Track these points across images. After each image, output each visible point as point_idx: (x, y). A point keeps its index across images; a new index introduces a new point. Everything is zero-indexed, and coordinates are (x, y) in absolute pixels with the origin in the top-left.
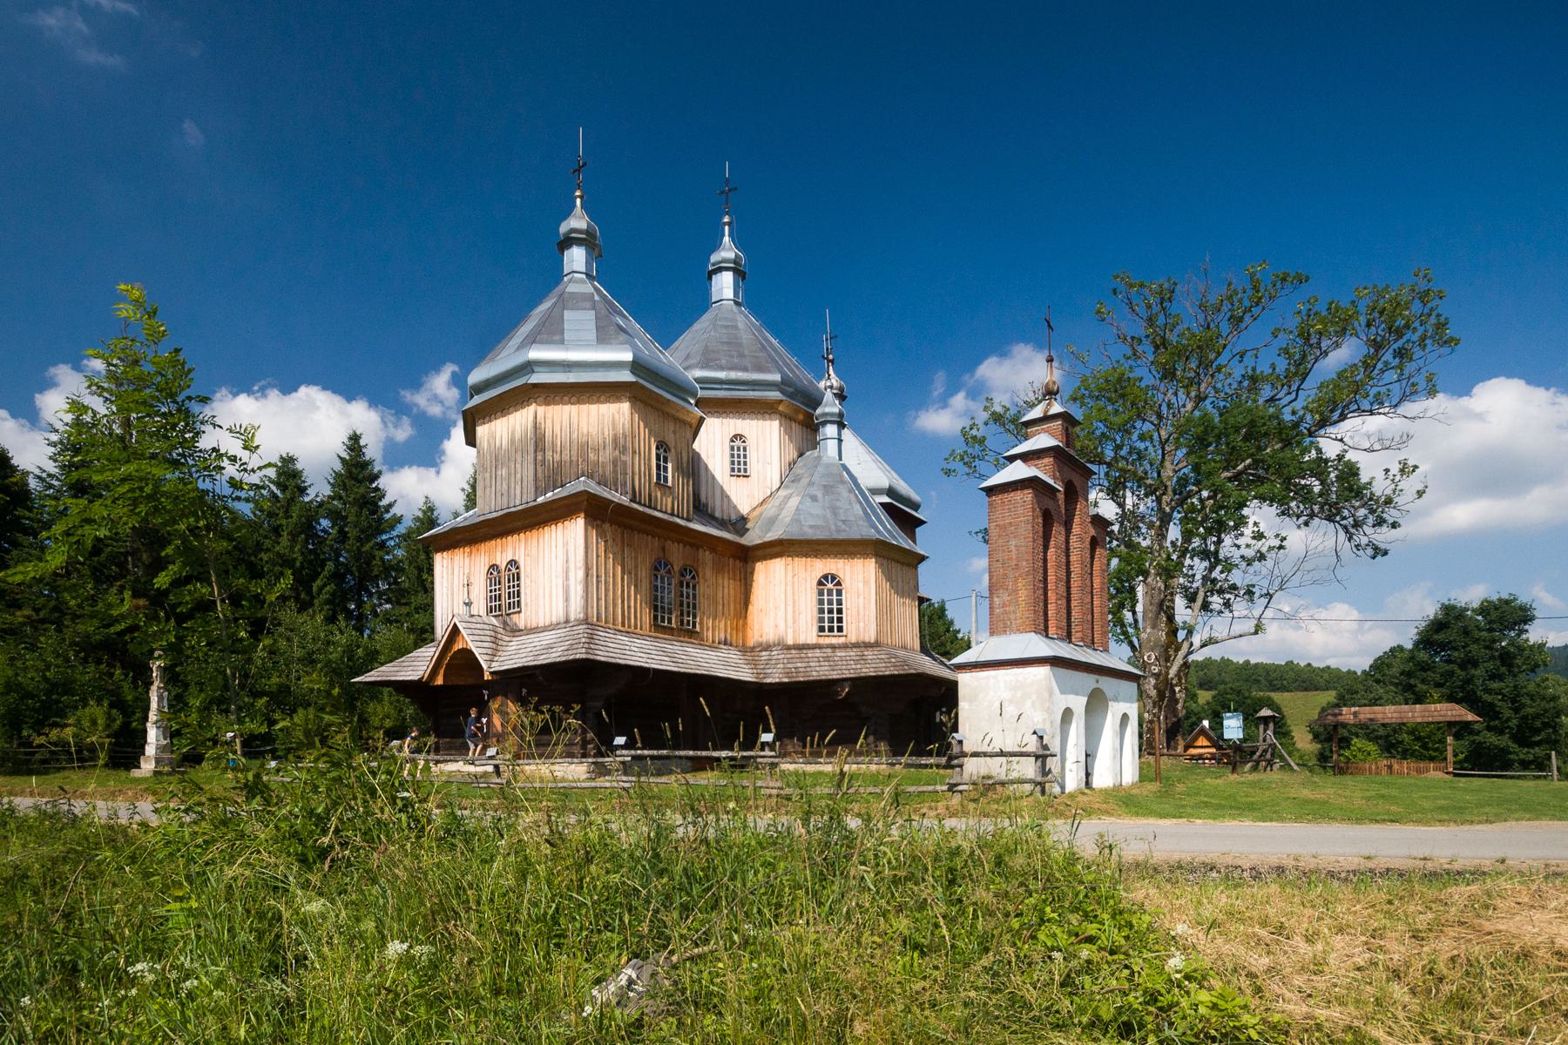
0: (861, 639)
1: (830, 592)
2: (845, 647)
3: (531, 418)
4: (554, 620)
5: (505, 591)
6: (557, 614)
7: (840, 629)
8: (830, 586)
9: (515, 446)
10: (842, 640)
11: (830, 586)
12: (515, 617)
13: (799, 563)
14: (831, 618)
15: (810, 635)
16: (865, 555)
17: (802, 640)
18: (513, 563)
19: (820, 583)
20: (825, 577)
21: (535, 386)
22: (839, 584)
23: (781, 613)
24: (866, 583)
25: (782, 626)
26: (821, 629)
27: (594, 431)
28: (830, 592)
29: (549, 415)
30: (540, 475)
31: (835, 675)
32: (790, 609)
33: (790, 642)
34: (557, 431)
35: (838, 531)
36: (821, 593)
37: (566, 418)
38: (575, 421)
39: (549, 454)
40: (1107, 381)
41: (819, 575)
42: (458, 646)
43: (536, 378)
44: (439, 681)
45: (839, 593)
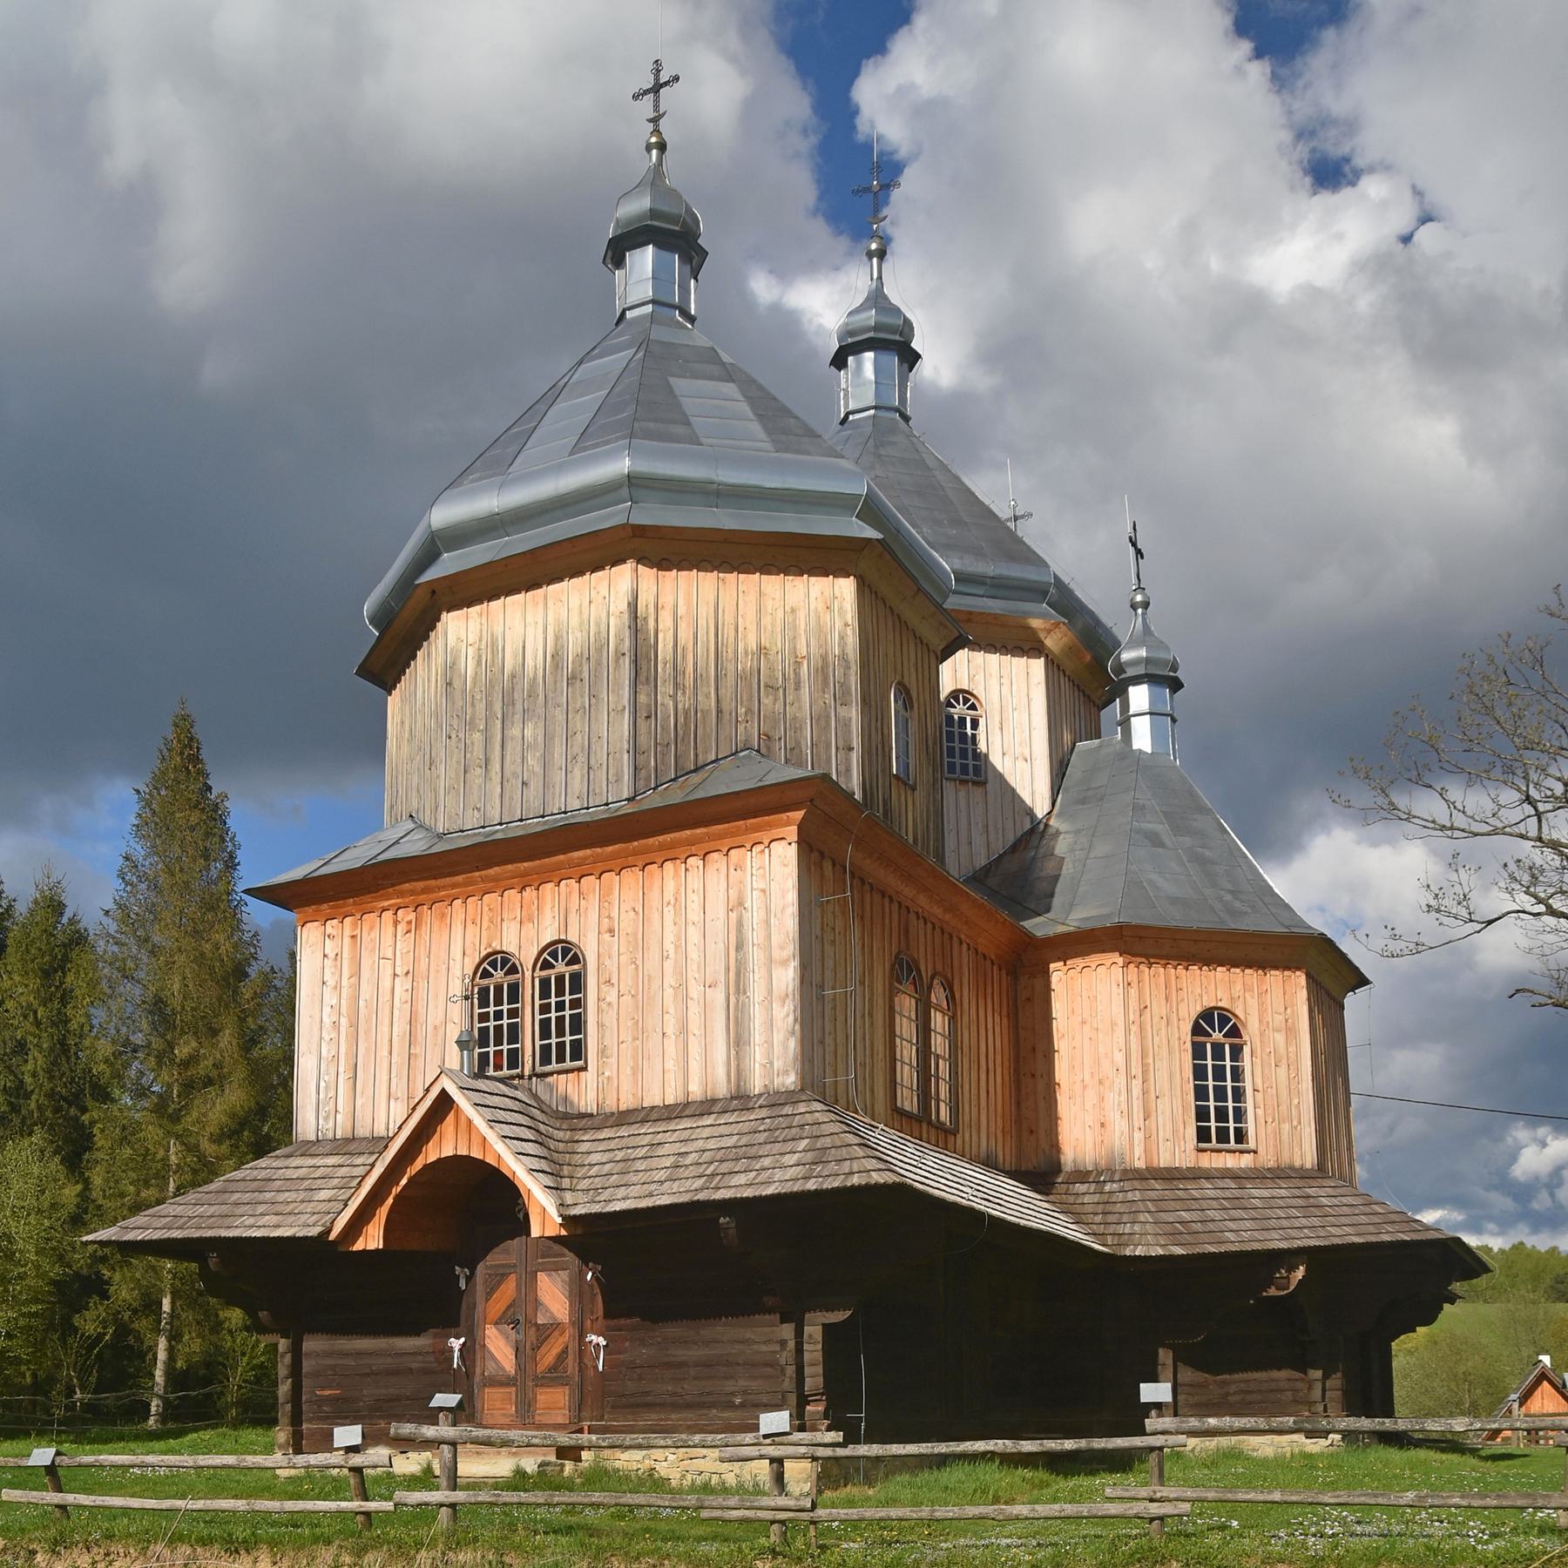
0: (1285, 1160)
1: (1218, 1052)
2: (1259, 1176)
3: (620, 604)
4: (696, 1091)
5: (529, 1019)
6: (707, 1073)
7: (1241, 1136)
8: (1217, 1036)
9: (572, 673)
10: (1246, 1161)
11: (1217, 1036)
12: (564, 1084)
13: (1157, 977)
14: (1218, 1114)
15: (1177, 1147)
16: (1286, 966)
17: (1164, 1160)
18: (563, 950)
19: (1197, 1030)
20: (1207, 1015)
21: (639, 531)
22: (1235, 1032)
23: (1115, 1099)
24: (1290, 1031)
25: (1119, 1125)
26: (1203, 1135)
27: (775, 643)
28: (1218, 1052)
29: (667, 599)
30: (643, 739)
31: (1277, 1242)
32: (1136, 1086)
33: (1140, 1164)
34: (685, 636)
35: (1233, 913)
36: (1198, 1051)
37: (705, 612)
38: (728, 618)
39: (666, 689)
40: (1491, 660)
41: (1209, 1002)
42: (444, 1146)
43: (449, 564)
44: (372, 1239)
45: (1237, 1052)
